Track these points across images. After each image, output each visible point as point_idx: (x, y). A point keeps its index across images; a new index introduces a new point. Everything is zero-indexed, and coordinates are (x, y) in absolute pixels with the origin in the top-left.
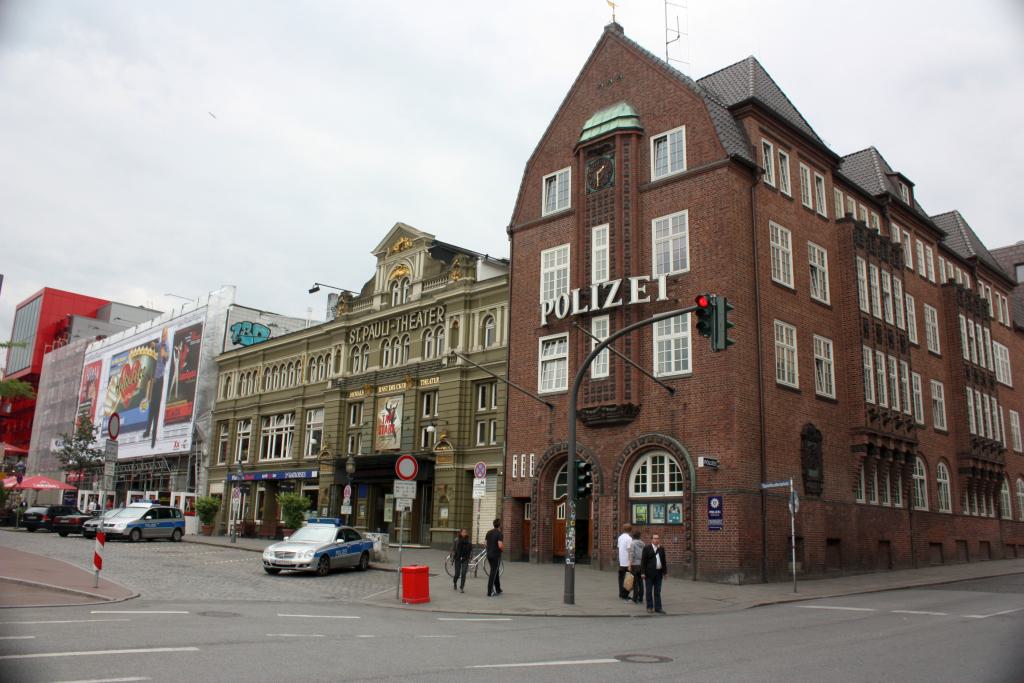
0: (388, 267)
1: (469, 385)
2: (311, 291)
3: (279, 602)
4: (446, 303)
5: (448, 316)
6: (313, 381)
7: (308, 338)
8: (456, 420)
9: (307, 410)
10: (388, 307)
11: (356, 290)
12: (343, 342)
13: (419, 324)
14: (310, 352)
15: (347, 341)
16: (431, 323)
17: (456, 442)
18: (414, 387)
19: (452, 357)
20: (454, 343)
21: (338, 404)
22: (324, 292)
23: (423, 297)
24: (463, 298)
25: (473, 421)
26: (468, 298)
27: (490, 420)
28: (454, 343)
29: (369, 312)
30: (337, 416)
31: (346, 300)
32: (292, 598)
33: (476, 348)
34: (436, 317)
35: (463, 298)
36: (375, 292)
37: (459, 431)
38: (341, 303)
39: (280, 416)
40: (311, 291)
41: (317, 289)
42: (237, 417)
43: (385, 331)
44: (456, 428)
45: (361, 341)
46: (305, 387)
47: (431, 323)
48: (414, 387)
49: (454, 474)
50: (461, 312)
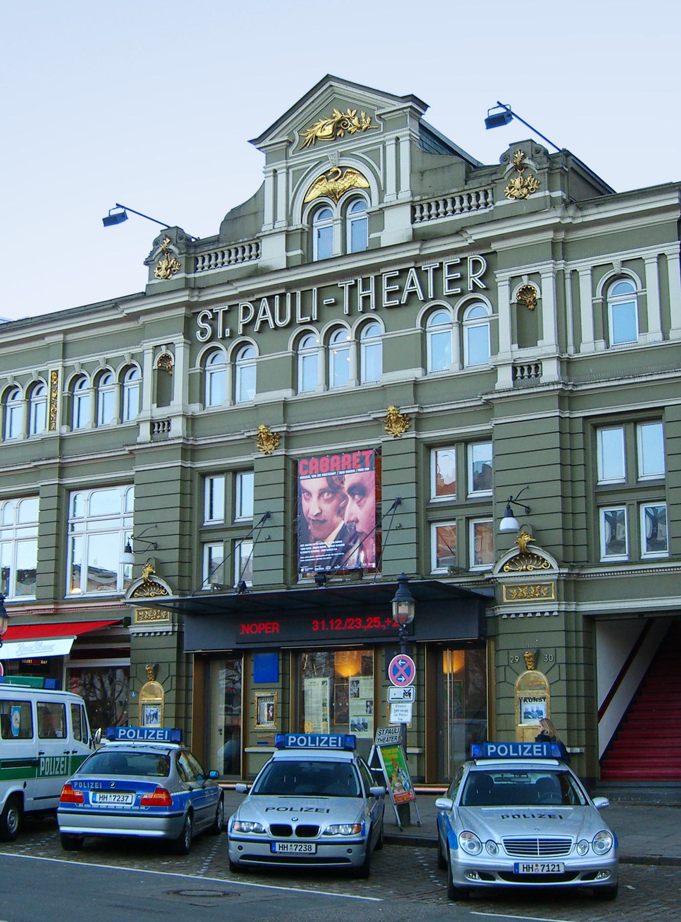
0: (298, 176)
1: (578, 427)
2: (110, 221)
3: (145, 910)
4: (494, 246)
5: (502, 276)
6: (85, 421)
7: (66, 332)
8: (175, 541)
9: (204, 475)
10: (306, 261)
11: (204, 225)
12: (179, 339)
13: (412, 294)
14: (69, 363)
15: (188, 333)
16: (446, 291)
17: (176, 580)
18: (281, 452)
19: (159, 426)
20: (162, 396)
21: (177, 474)
22: (513, 133)
23: (419, 237)
24: (550, 235)
25: (422, 521)
26: (561, 235)
27: (468, 519)
28: (162, 396)
29: (258, 272)
30: (176, 500)
31: (178, 248)
32: (119, 903)
33: (589, 346)
34: (463, 279)
35: (550, 235)
36: (267, 228)
37: (181, 562)
38: (166, 251)
39: (464, 443)
40: (110, 221)
41: (122, 217)
42: (67, 481)
43: (282, 318)
44: (175, 555)
45: (233, 336)
46: (62, 439)
47: (446, 291)
48: (281, 452)
49: (560, 624)
50: (546, 269)
